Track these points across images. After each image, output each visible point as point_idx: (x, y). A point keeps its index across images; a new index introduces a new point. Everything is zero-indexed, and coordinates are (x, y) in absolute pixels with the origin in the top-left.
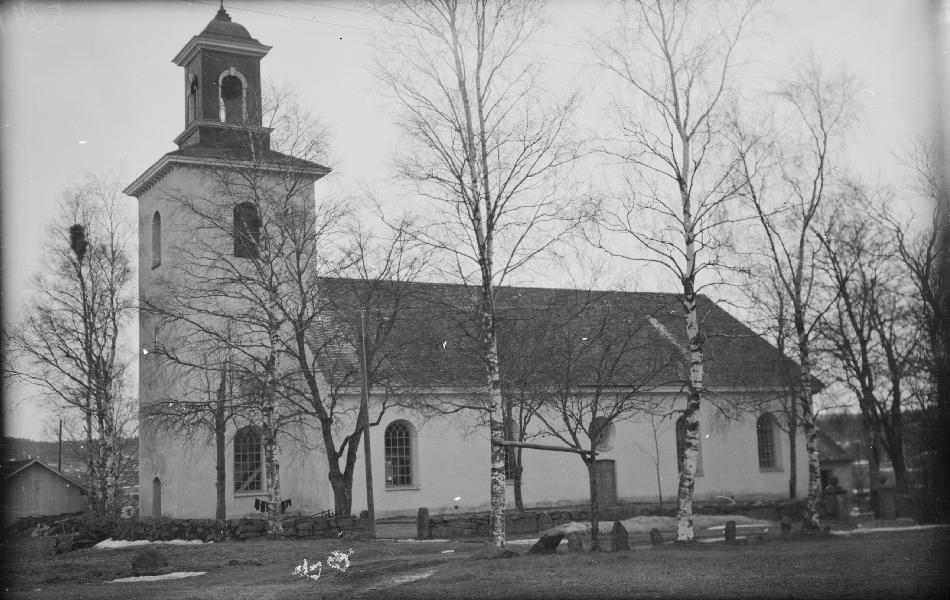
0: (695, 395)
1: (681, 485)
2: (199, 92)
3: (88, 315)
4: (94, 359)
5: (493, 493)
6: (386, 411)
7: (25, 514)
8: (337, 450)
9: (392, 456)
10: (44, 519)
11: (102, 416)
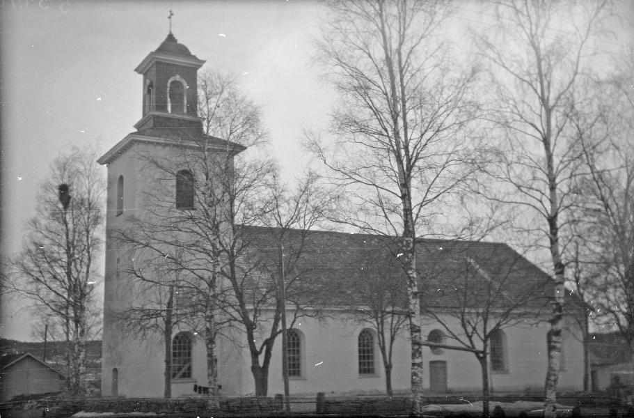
0: (559, 308)
1: (548, 379)
2: (153, 91)
3: (70, 246)
4: (73, 279)
5: (413, 383)
6: (297, 319)
7: (18, 393)
8: (258, 349)
9: (370, 348)
10: (34, 397)
11: (77, 321)
